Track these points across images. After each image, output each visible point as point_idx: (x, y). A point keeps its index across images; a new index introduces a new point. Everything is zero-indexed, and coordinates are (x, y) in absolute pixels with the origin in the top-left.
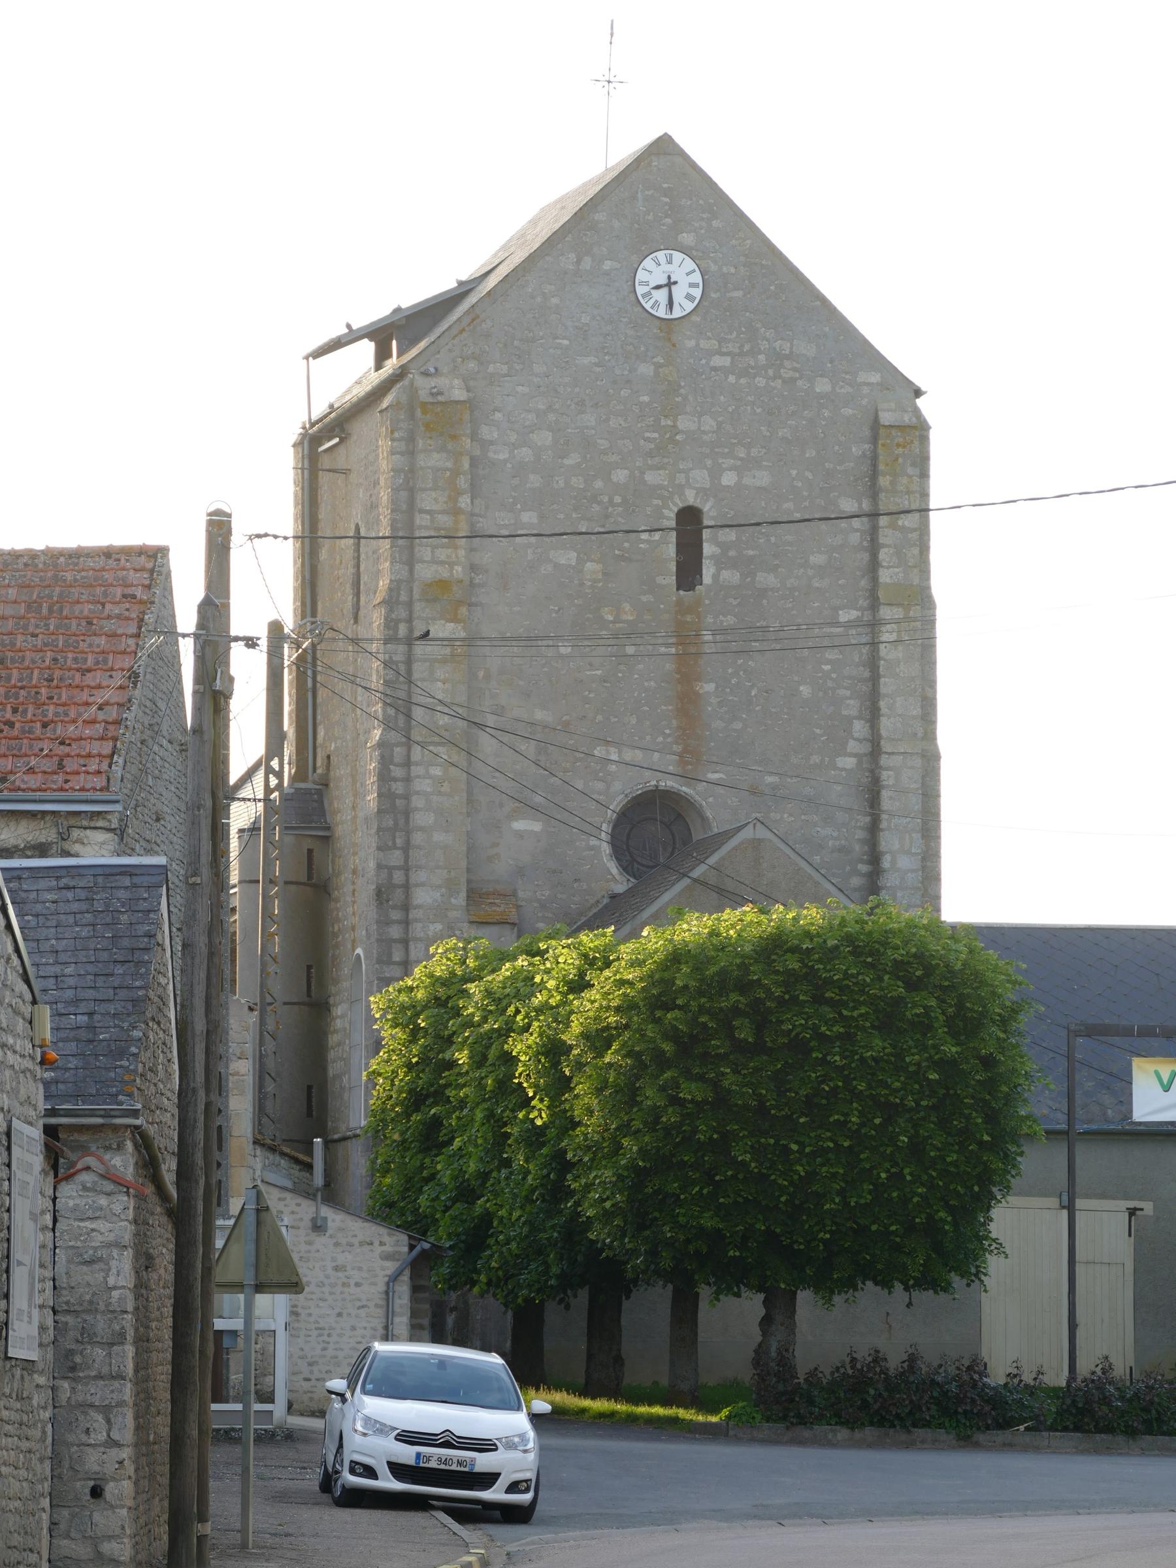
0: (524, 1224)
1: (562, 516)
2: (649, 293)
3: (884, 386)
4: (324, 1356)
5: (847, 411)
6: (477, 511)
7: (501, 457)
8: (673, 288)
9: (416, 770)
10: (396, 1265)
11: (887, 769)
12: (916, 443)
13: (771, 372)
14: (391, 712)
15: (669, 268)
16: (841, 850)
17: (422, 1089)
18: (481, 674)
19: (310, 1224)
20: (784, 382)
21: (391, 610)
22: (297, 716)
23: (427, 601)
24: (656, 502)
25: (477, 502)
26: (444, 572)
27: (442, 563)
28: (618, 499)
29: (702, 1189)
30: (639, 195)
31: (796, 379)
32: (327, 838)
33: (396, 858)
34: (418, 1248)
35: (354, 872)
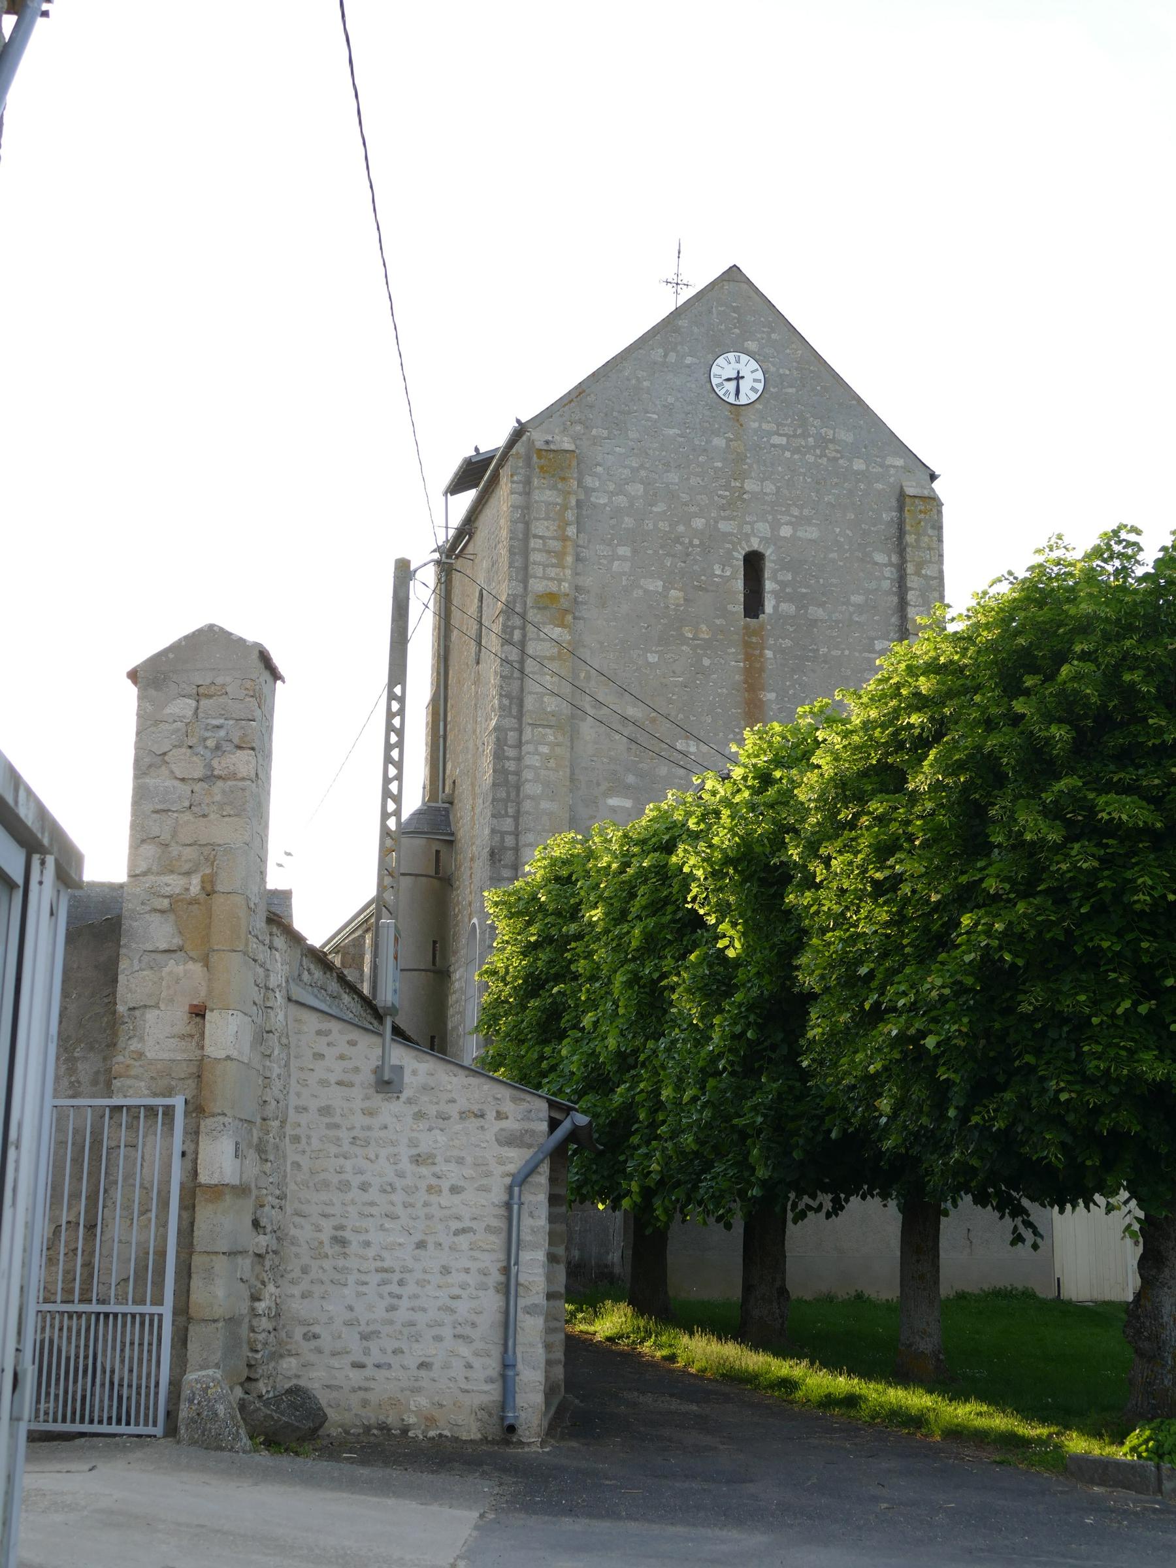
0: (704, 1106)
1: (650, 552)
2: (722, 384)
3: (907, 469)
4: (391, 1322)
5: (879, 486)
6: (581, 542)
7: (602, 501)
9: (527, 748)
10: (527, 1154)
12: (935, 511)
14: (506, 702)
15: (738, 366)
17: (542, 971)
19: (371, 1078)
20: (829, 459)
21: (508, 619)
22: (432, 757)
23: (539, 608)
24: (728, 546)
25: (581, 535)
26: (553, 587)
27: (552, 579)
29: (1136, 1004)
32: (451, 842)
33: (508, 824)
34: (566, 1126)
35: (472, 859)
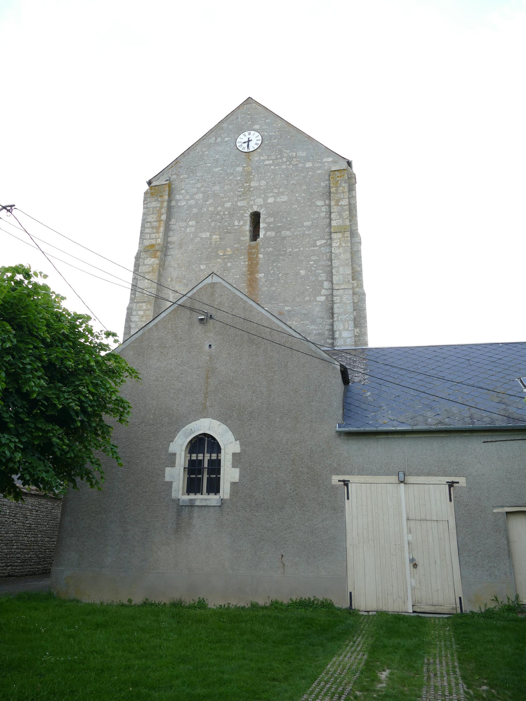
1: (204, 221)
7: (183, 204)
8: (250, 143)
11: (336, 296)
13: (288, 163)
16: (319, 334)
18: (169, 279)
20: (293, 165)
23: (145, 252)
26: (153, 242)
27: (153, 239)
28: (227, 213)
30: (239, 117)
31: (298, 164)
